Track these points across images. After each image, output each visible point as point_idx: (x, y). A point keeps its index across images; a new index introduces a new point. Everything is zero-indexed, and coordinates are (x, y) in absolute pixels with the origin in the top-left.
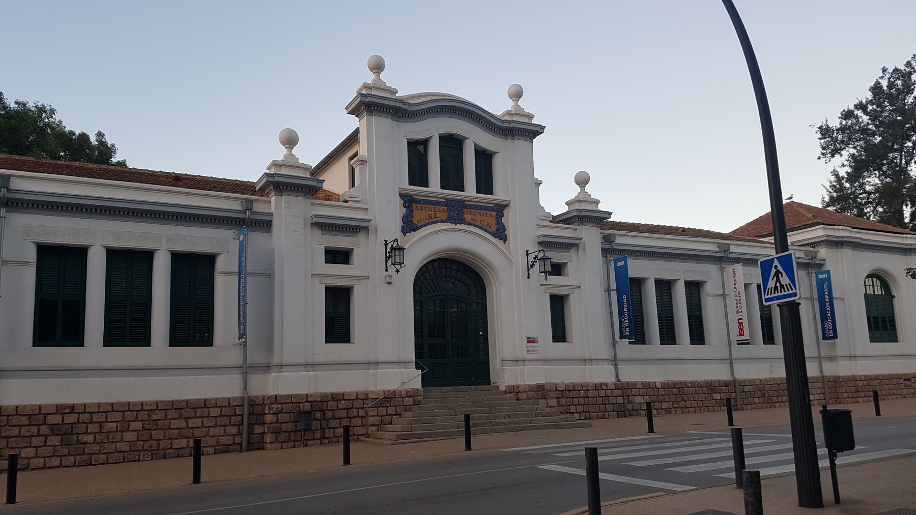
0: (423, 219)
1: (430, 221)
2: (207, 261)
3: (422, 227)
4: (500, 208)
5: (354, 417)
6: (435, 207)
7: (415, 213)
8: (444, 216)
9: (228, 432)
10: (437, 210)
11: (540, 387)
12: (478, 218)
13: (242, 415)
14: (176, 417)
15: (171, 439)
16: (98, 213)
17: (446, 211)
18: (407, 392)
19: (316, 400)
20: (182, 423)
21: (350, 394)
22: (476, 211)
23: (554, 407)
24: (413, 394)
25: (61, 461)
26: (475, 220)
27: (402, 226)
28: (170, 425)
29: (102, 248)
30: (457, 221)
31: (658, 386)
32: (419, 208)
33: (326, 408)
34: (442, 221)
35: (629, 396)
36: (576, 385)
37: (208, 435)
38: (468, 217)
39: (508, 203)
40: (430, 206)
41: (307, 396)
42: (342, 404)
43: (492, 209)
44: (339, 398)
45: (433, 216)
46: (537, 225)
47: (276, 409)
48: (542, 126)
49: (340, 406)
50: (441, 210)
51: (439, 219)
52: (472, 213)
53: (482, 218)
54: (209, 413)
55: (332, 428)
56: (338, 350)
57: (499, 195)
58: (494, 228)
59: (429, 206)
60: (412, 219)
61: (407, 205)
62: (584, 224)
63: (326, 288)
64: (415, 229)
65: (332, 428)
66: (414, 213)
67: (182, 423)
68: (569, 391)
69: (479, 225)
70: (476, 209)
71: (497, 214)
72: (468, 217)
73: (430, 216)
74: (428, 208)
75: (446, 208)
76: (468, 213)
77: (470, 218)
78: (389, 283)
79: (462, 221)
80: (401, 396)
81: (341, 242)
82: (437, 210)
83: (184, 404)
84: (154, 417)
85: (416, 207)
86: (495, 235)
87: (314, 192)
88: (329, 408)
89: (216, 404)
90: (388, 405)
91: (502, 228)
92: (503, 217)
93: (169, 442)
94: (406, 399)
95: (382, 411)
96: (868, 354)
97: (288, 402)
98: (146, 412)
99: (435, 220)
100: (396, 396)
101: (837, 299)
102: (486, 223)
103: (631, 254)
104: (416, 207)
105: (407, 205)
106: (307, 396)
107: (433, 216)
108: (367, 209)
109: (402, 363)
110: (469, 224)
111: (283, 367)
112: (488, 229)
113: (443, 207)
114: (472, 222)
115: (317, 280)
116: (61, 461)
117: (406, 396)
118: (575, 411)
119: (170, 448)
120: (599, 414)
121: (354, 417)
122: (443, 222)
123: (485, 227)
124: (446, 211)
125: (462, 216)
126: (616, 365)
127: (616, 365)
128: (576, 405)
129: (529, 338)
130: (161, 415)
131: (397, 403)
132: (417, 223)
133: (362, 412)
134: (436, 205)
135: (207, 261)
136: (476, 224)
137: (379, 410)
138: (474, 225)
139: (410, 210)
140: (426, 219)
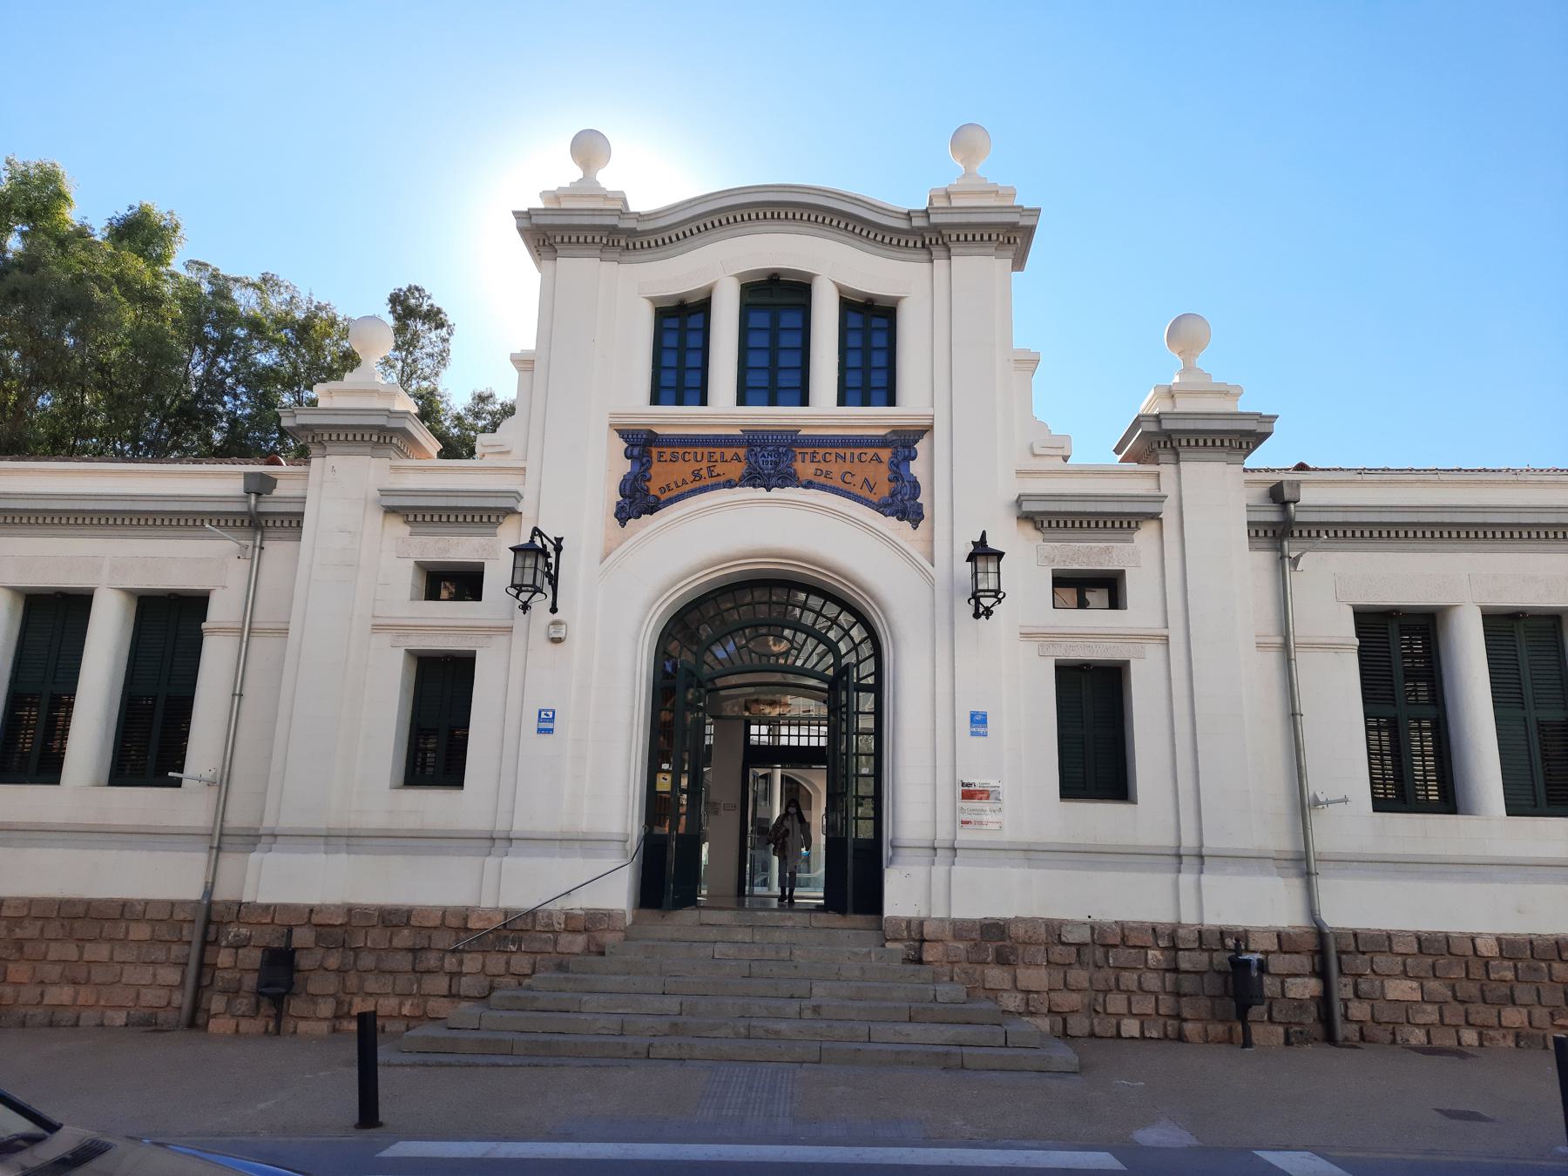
0: (676, 483)
1: (697, 485)
2: (194, 605)
3: (671, 501)
4: (904, 442)
5: (429, 972)
6: (711, 450)
7: (656, 469)
8: (736, 470)
9: (160, 980)
10: (717, 456)
11: (993, 931)
12: (836, 468)
13: (189, 943)
14: (60, 937)
15: (42, 982)
16: (158, 526)
17: (743, 458)
18: (569, 916)
19: (331, 922)
20: (71, 952)
21: (426, 911)
22: (828, 450)
23: (1037, 992)
24: (593, 922)
25: (237, 1025)
26: (827, 475)
27: (618, 503)
28: (46, 953)
29: (118, 592)
30: (773, 481)
31: (557, 927)
32: (667, 456)
33: (362, 945)
34: (730, 484)
35: (1360, 976)
36: (1132, 929)
37: (119, 981)
38: (805, 469)
39: (927, 422)
40: (699, 450)
41: (312, 910)
42: (404, 938)
43: (882, 442)
44: (394, 922)
45: (704, 473)
46: (1018, 472)
47: (235, 936)
48: (1024, 210)
49: (397, 943)
50: (868, 457)
51: (722, 479)
52: (819, 457)
53: (847, 467)
54: (127, 932)
55: (371, 994)
56: (432, 805)
57: (912, 403)
58: (884, 490)
59: (695, 450)
60: (647, 484)
61: (636, 451)
62: (329, 449)
63: (1056, 667)
64: (652, 509)
65: (371, 994)
66: (652, 471)
67: (71, 952)
68: (1107, 947)
69: (837, 485)
70: (831, 447)
71: (895, 455)
72: (805, 469)
73: (697, 475)
74: (692, 456)
75: (742, 452)
76: (808, 457)
77: (813, 471)
78: (557, 641)
79: (787, 479)
80: (551, 929)
81: (458, 548)
82: (717, 456)
83: (80, 910)
84: (19, 933)
85: (660, 455)
86: (884, 508)
87: (1251, 447)
88: (369, 944)
89: (144, 914)
90: (514, 949)
91: (907, 490)
92: (914, 459)
93: (38, 990)
94: (565, 939)
95: (496, 963)
96: (1004, 852)
97: (264, 921)
98: (5, 923)
99: (710, 481)
100: (538, 928)
101: (1336, 647)
102: (858, 480)
103: (13, 523)
104: (660, 455)
105: (636, 451)
106: (312, 910)
107: (704, 473)
108: (524, 469)
109: (577, 844)
110: (809, 485)
111: (278, 838)
112: (865, 493)
113: (734, 450)
114: (816, 480)
115: (385, 639)
116: (237, 1025)
117: (565, 930)
118: (1125, 1011)
119: (38, 1004)
120: (1210, 1027)
121: (429, 972)
122: (732, 487)
123: (857, 491)
124: (743, 458)
125: (789, 467)
126: (1308, 876)
127: (1308, 876)
128: (1129, 992)
129: (969, 785)
130: (31, 930)
131: (536, 946)
132: (658, 494)
133: (450, 963)
134: (714, 446)
135: (194, 605)
136: (829, 483)
137: (240, 956)
138: (823, 488)
139: (643, 465)
140: (684, 482)
